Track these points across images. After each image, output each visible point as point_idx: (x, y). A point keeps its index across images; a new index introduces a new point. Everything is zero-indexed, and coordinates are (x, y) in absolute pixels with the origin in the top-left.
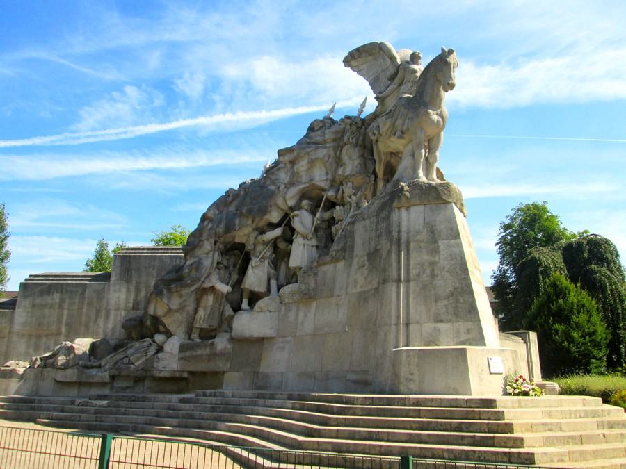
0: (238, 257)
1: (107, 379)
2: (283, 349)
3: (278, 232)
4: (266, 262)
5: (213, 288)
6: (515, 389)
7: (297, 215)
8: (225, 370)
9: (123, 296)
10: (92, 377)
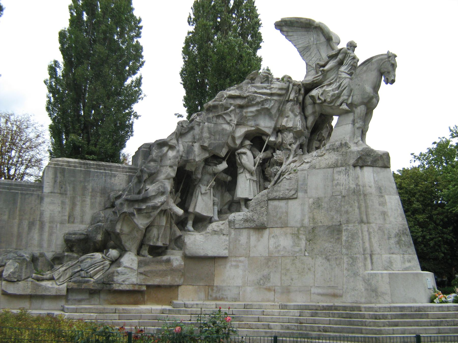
0: (185, 183)
1: (64, 292)
2: (237, 266)
6: (287, 291)
9: (57, 209)
10: (46, 288)
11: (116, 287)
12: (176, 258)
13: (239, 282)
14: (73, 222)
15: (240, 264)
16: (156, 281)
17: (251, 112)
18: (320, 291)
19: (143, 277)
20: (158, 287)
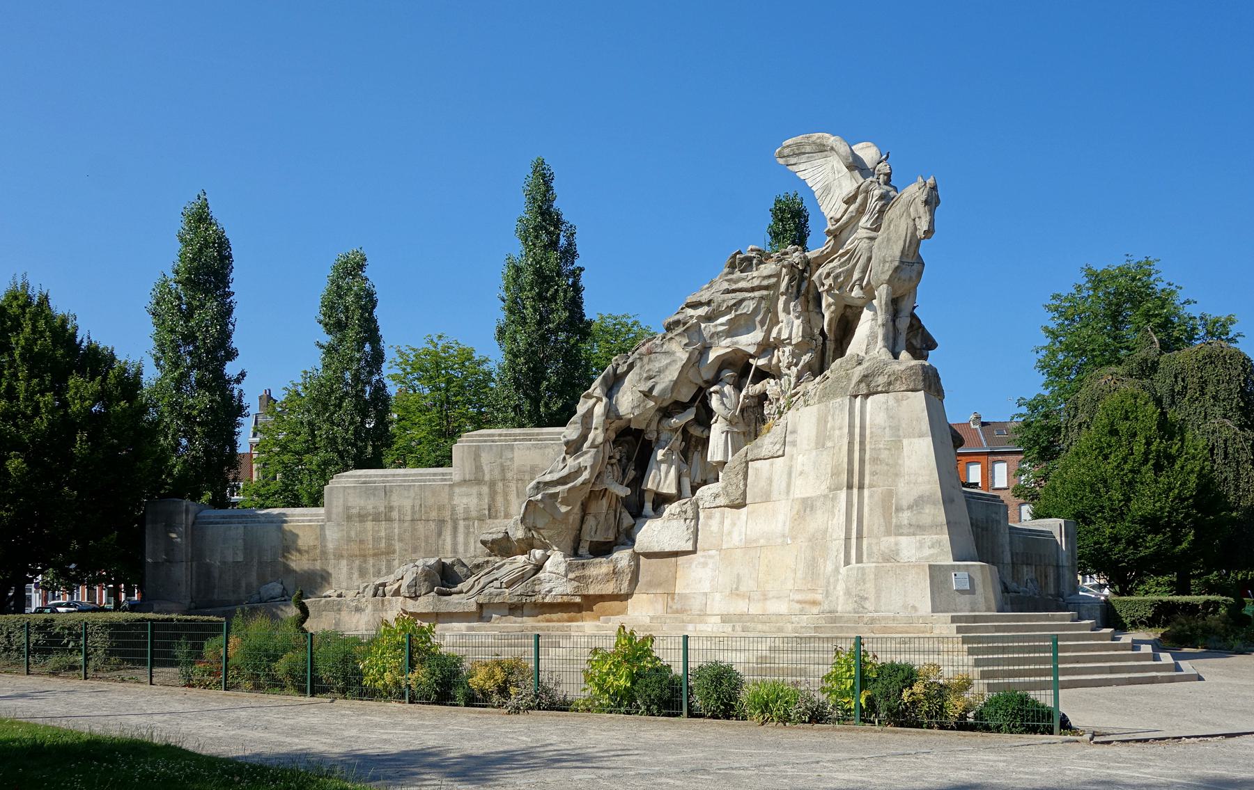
2: (705, 565)
13: (706, 587)
14: (496, 517)
15: (710, 561)
17: (722, 324)
18: (799, 597)
20: (602, 598)
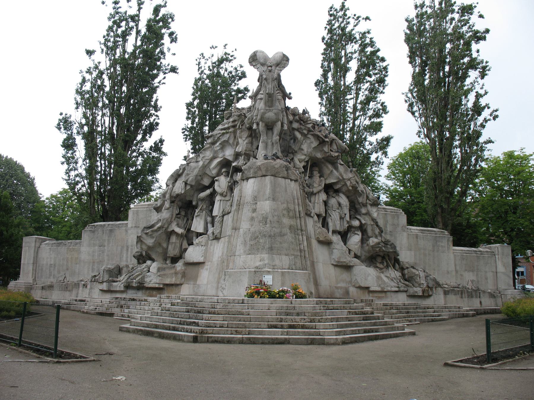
3: (208, 192)
4: (204, 212)
5: (173, 232)
7: (217, 180)
8: (181, 282)
11: (146, 285)
12: (179, 265)
16: (168, 281)
19: (160, 278)
20: (172, 285)
